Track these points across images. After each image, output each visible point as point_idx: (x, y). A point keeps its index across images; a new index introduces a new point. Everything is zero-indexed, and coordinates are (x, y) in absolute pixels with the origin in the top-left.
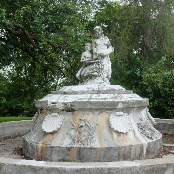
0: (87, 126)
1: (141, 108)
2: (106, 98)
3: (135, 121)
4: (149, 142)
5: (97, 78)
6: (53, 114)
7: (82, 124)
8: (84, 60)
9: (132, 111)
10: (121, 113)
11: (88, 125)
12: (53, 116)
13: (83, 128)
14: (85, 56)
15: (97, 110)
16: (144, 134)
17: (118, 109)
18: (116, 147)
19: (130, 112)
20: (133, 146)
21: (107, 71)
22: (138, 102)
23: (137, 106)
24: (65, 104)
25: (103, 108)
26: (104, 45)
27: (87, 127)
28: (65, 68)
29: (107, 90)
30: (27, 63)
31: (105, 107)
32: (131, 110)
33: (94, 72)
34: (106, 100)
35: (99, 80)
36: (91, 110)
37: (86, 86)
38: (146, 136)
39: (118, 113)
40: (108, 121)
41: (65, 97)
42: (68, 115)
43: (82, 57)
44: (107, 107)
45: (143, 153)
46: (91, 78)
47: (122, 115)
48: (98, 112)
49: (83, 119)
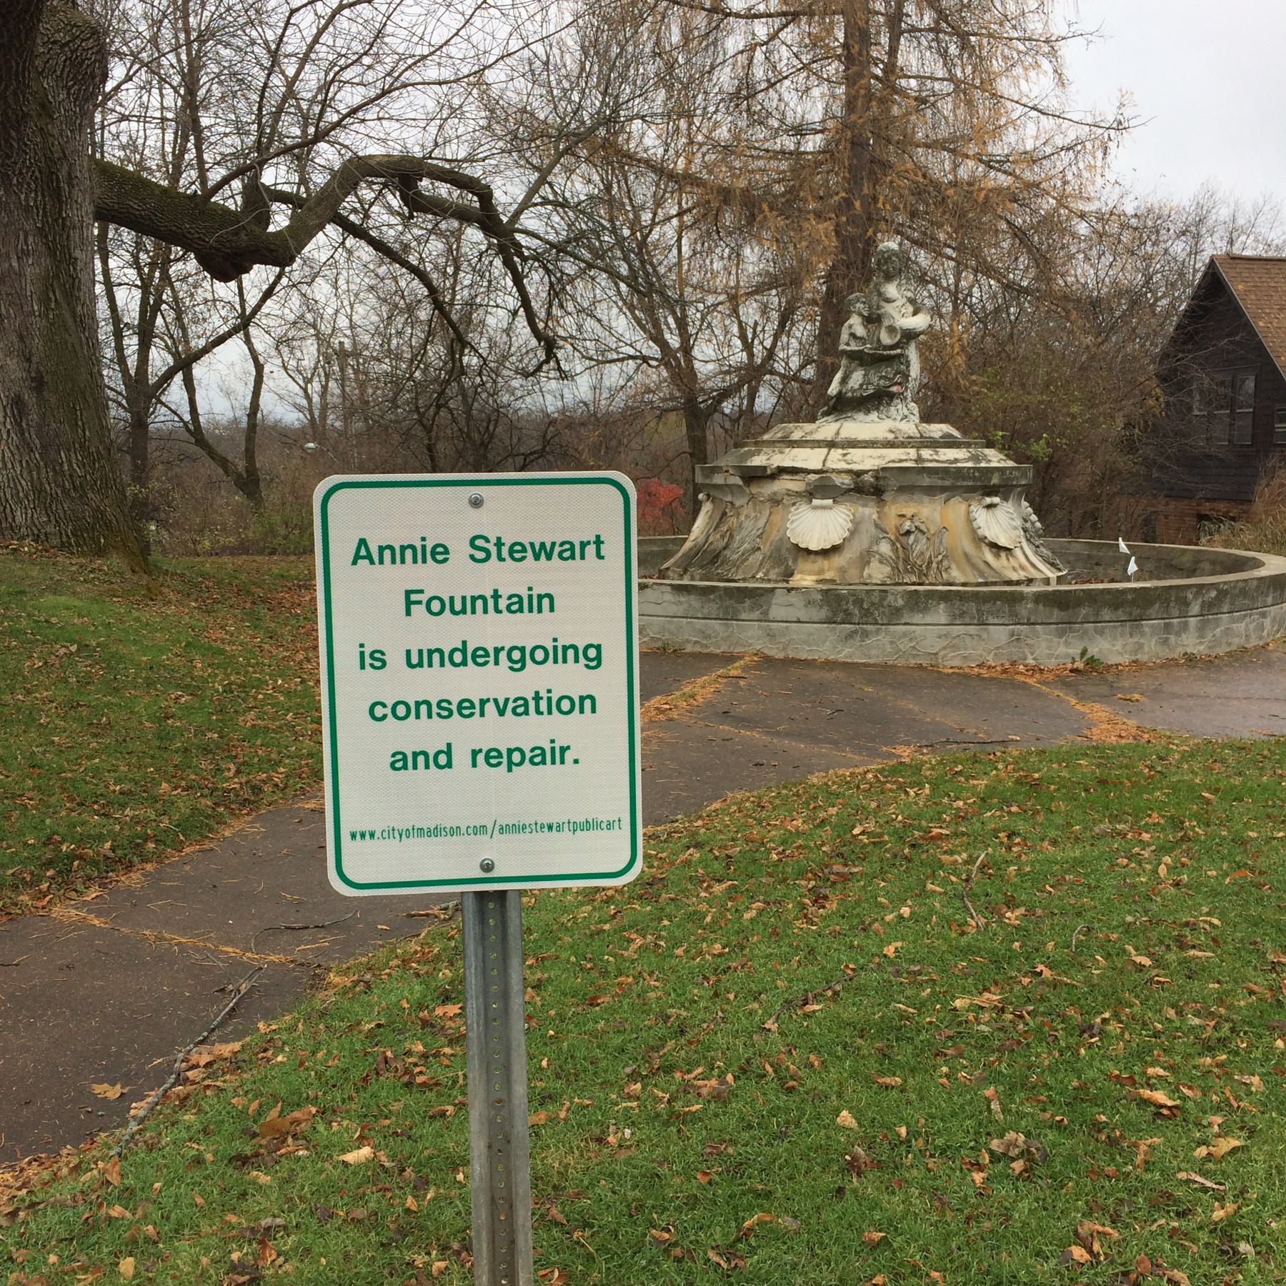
0: (921, 531)
2: (956, 461)
5: (896, 401)
6: (816, 502)
7: (907, 525)
8: (848, 344)
11: (923, 528)
12: (816, 508)
13: (912, 537)
15: (943, 489)
24: (858, 474)
27: (919, 535)
30: (301, 1153)
35: (898, 409)
36: (931, 491)
37: (889, 424)
40: (970, 521)
41: (845, 455)
42: (865, 506)
43: (845, 336)
48: (944, 496)
49: (909, 514)
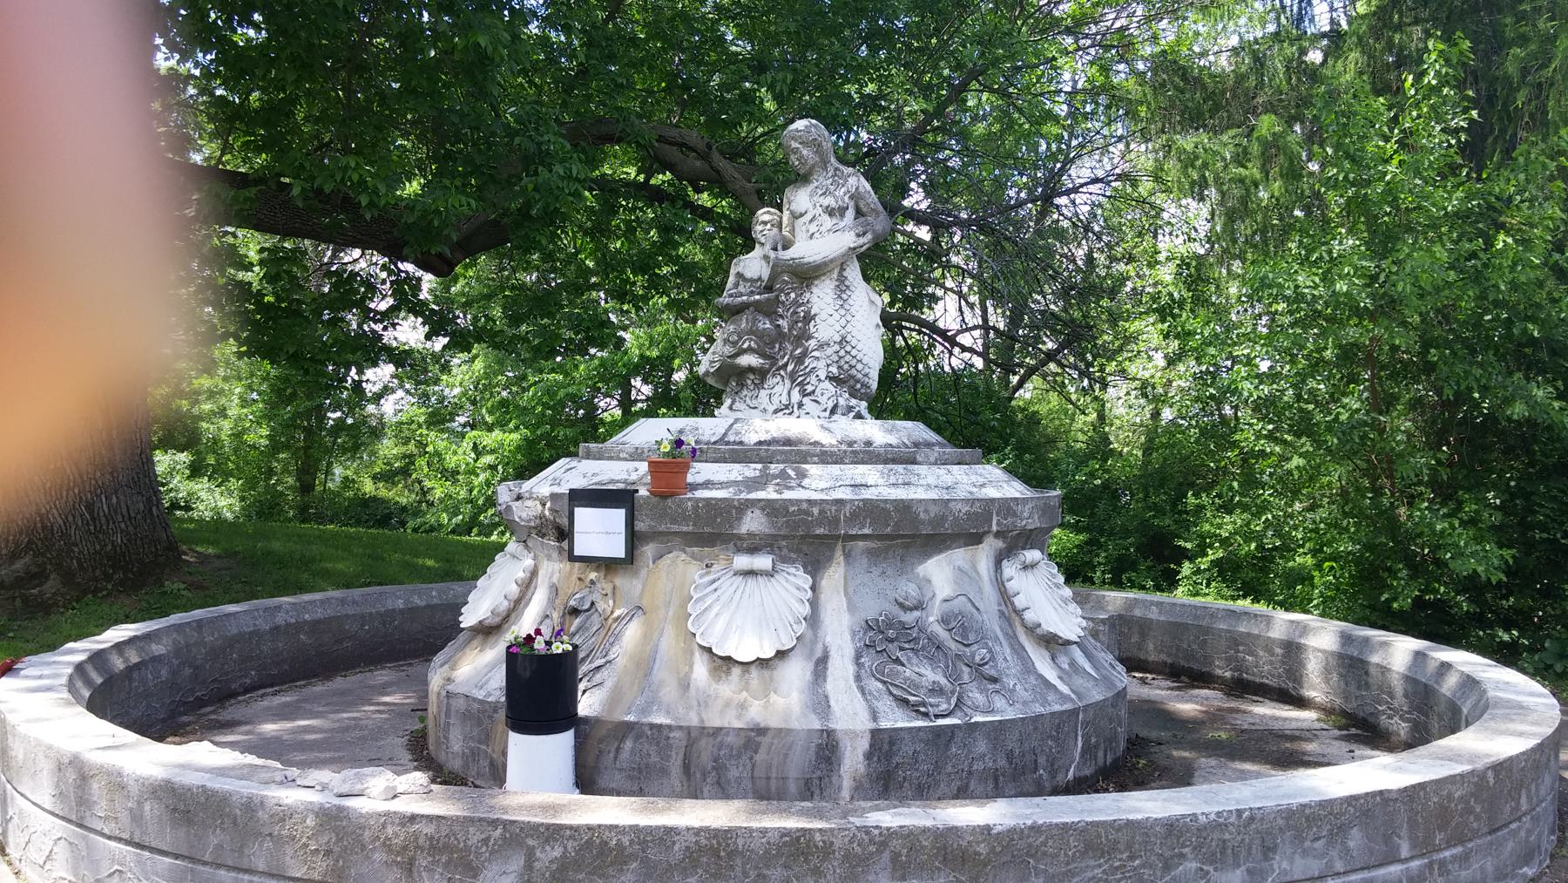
1: (1016, 542)
3: (851, 608)
4: (885, 724)
9: (839, 556)
10: (763, 561)
14: (739, 275)
16: (884, 683)
17: (740, 537)
18: (669, 727)
19: (830, 559)
20: (770, 734)
21: (837, 347)
22: (1006, 507)
23: (866, 531)
25: (662, 528)
26: (826, 217)
28: (1404, 324)
29: (760, 443)
31: (675, 528)
32: (833, 550)
33: (742, 352)
34: (610, 487)
38: (891, 693)
39: (742, 561)
44: (685, 529)
45: (834, 779)
46: (742, 385)
47: (770, 574)
